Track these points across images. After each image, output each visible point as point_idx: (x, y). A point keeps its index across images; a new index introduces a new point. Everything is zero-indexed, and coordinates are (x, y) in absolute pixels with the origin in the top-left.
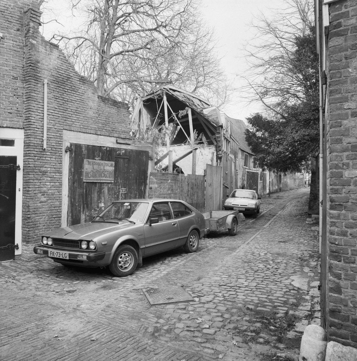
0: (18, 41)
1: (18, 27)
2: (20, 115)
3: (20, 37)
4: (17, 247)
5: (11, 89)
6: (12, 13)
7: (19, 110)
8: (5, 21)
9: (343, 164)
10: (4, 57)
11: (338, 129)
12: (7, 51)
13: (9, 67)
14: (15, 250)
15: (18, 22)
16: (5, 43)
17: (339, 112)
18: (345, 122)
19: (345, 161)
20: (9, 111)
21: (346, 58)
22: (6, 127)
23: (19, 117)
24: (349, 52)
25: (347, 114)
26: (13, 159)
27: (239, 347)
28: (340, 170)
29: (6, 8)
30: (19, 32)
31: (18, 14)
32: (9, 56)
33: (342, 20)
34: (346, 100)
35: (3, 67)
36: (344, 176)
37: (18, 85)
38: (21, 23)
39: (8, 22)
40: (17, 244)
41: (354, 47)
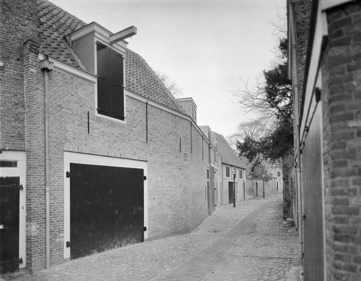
0: (18, 69)
1: (18, 57)
2: (22, 138)
3: (20, 67)
4: (21, 261)
5: (12, 114)
6: (12, 44)
7: (21, 133)
8: (5, 52)
9: (349, 190)
10: (5, 85)
11: (341, 150)
12: (8, 79)
13: (11, 94)
14: (20, 263)
15: (18, 53)
16: (6, 72)
17: (343, 131)
18: (350, 142)
19: (351, 186)
20: (11, 135)
21: (349, 70)
22: (9, 150)
23: (21, 141)
24: (353, 63)
25: (352, 134)
26: (17, 179)
27: (247, 256)
28: (345, 197)
29: (6, 40)
30: (19, 62)
31: (18, 45)
32: (11, 83)
33: (343, 28)
34: (350, 117)
35: (5, 94)
36: (350, 204)
37: (19, 110)
38: (21, 53)
39: (8, 52)
40: (21, 258)
41: (357, 57)
